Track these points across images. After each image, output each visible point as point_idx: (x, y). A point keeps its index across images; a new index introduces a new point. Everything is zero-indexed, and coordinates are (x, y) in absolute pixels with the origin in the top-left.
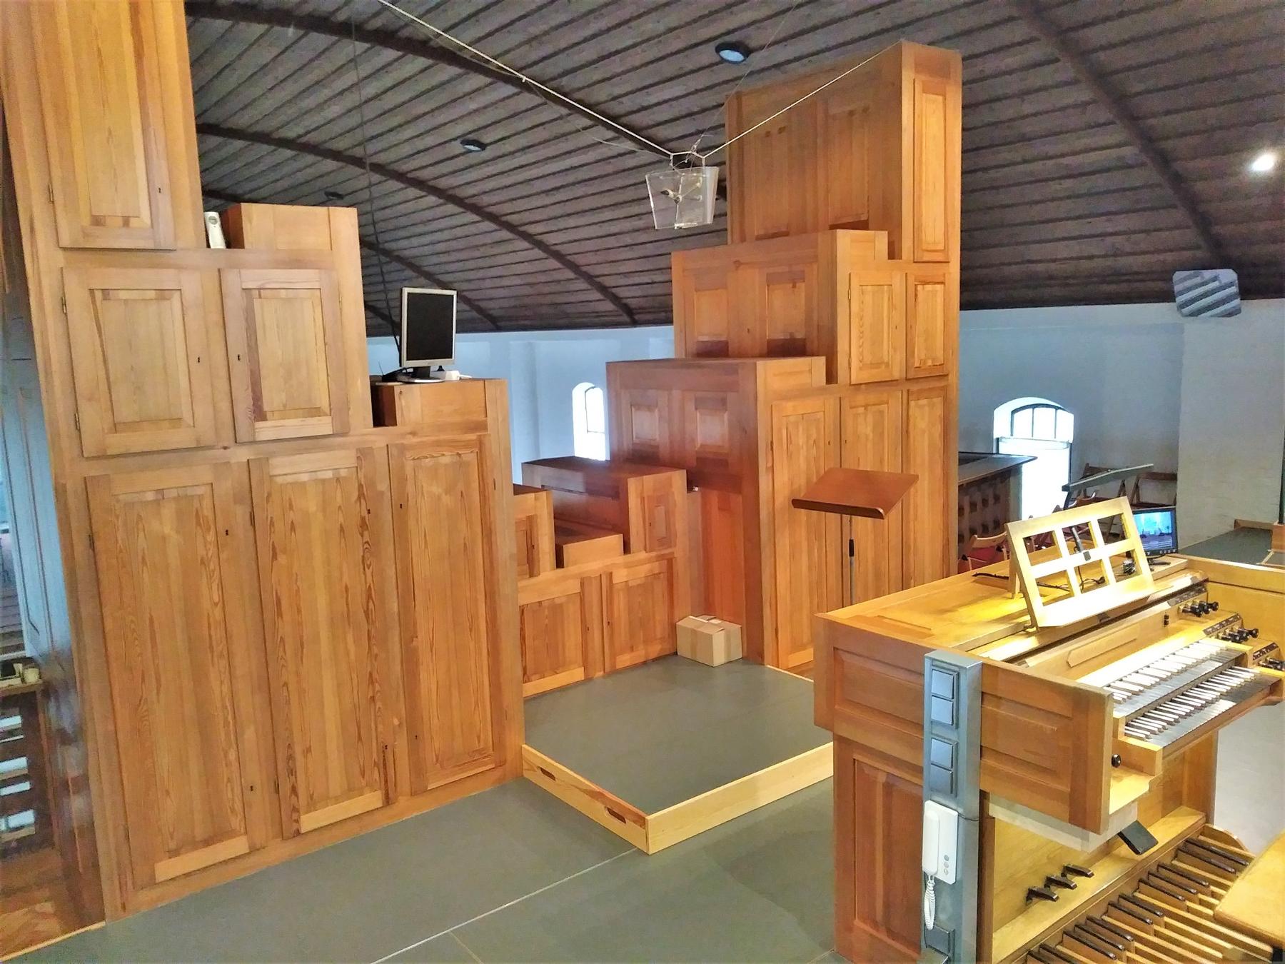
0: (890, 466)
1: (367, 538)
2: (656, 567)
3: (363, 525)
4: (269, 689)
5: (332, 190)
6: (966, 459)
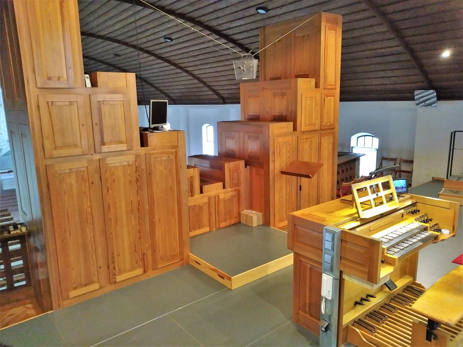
0: (314, 160)
1: (138, 185)
2: (234, 193)
3: (137, 180)
5: (116, 53)
6: (340, 155)
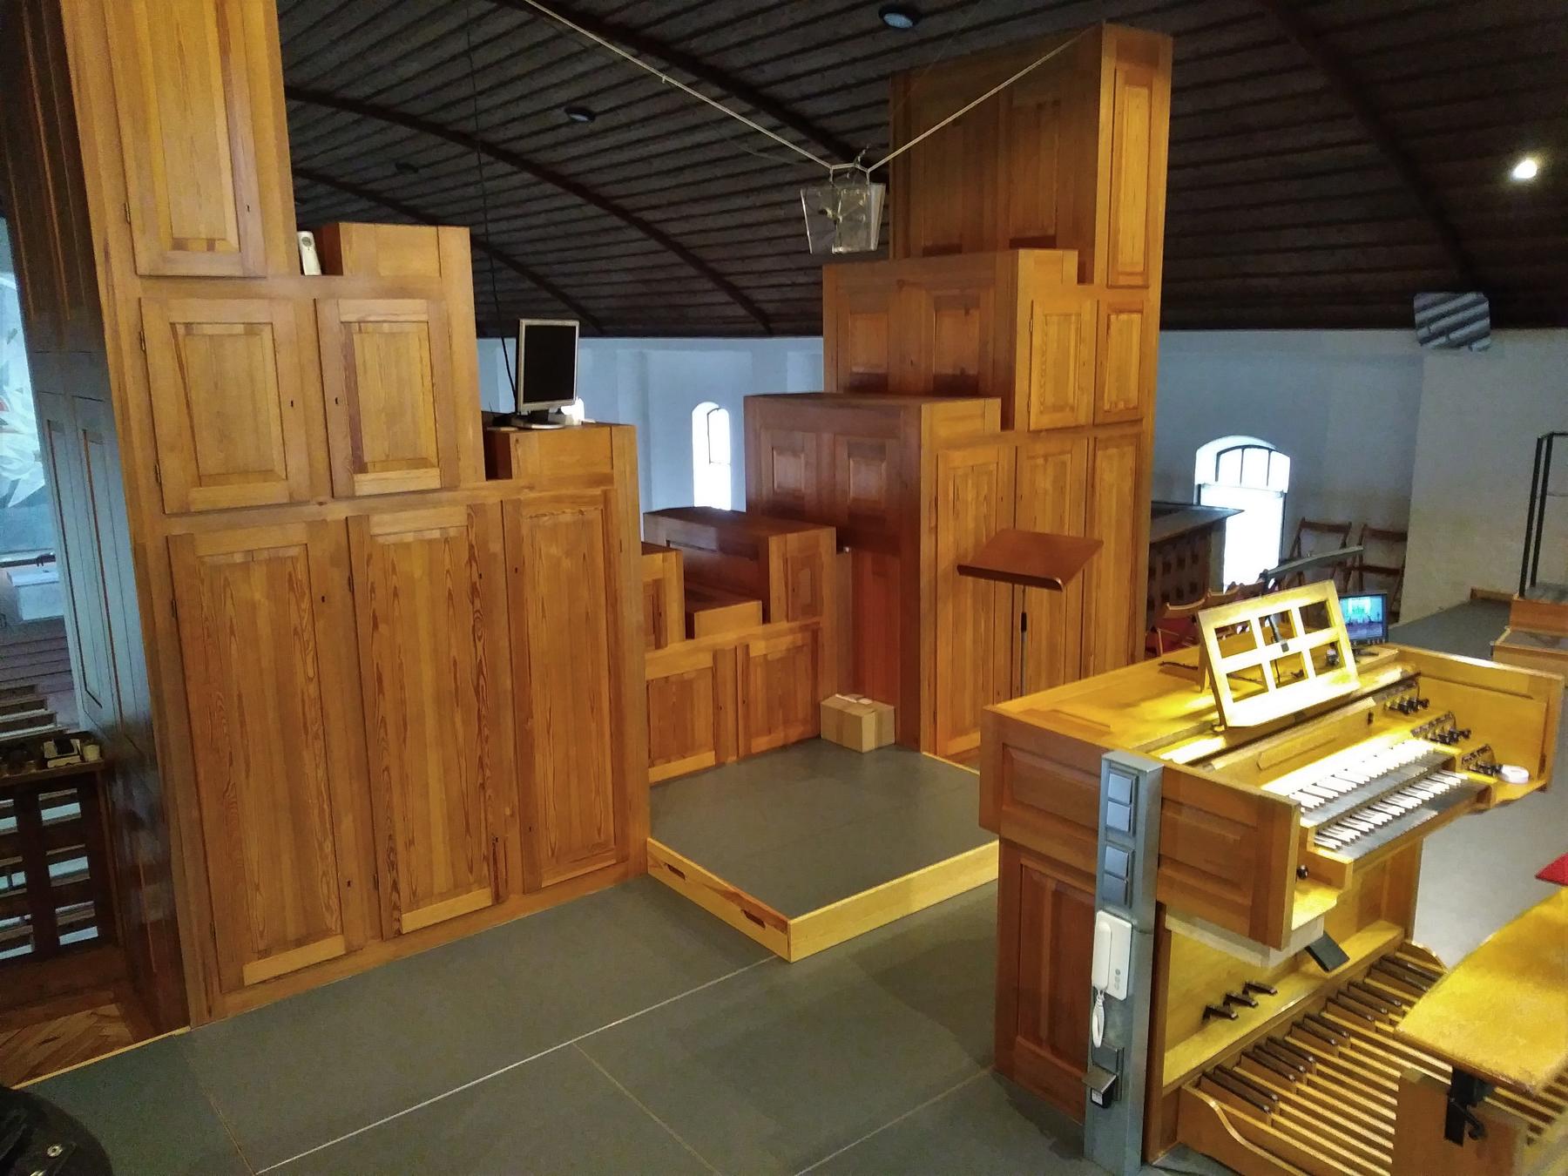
0: (1072, 529)
2: (799, 638)
3: (474, 591)
4: (367, 773)
